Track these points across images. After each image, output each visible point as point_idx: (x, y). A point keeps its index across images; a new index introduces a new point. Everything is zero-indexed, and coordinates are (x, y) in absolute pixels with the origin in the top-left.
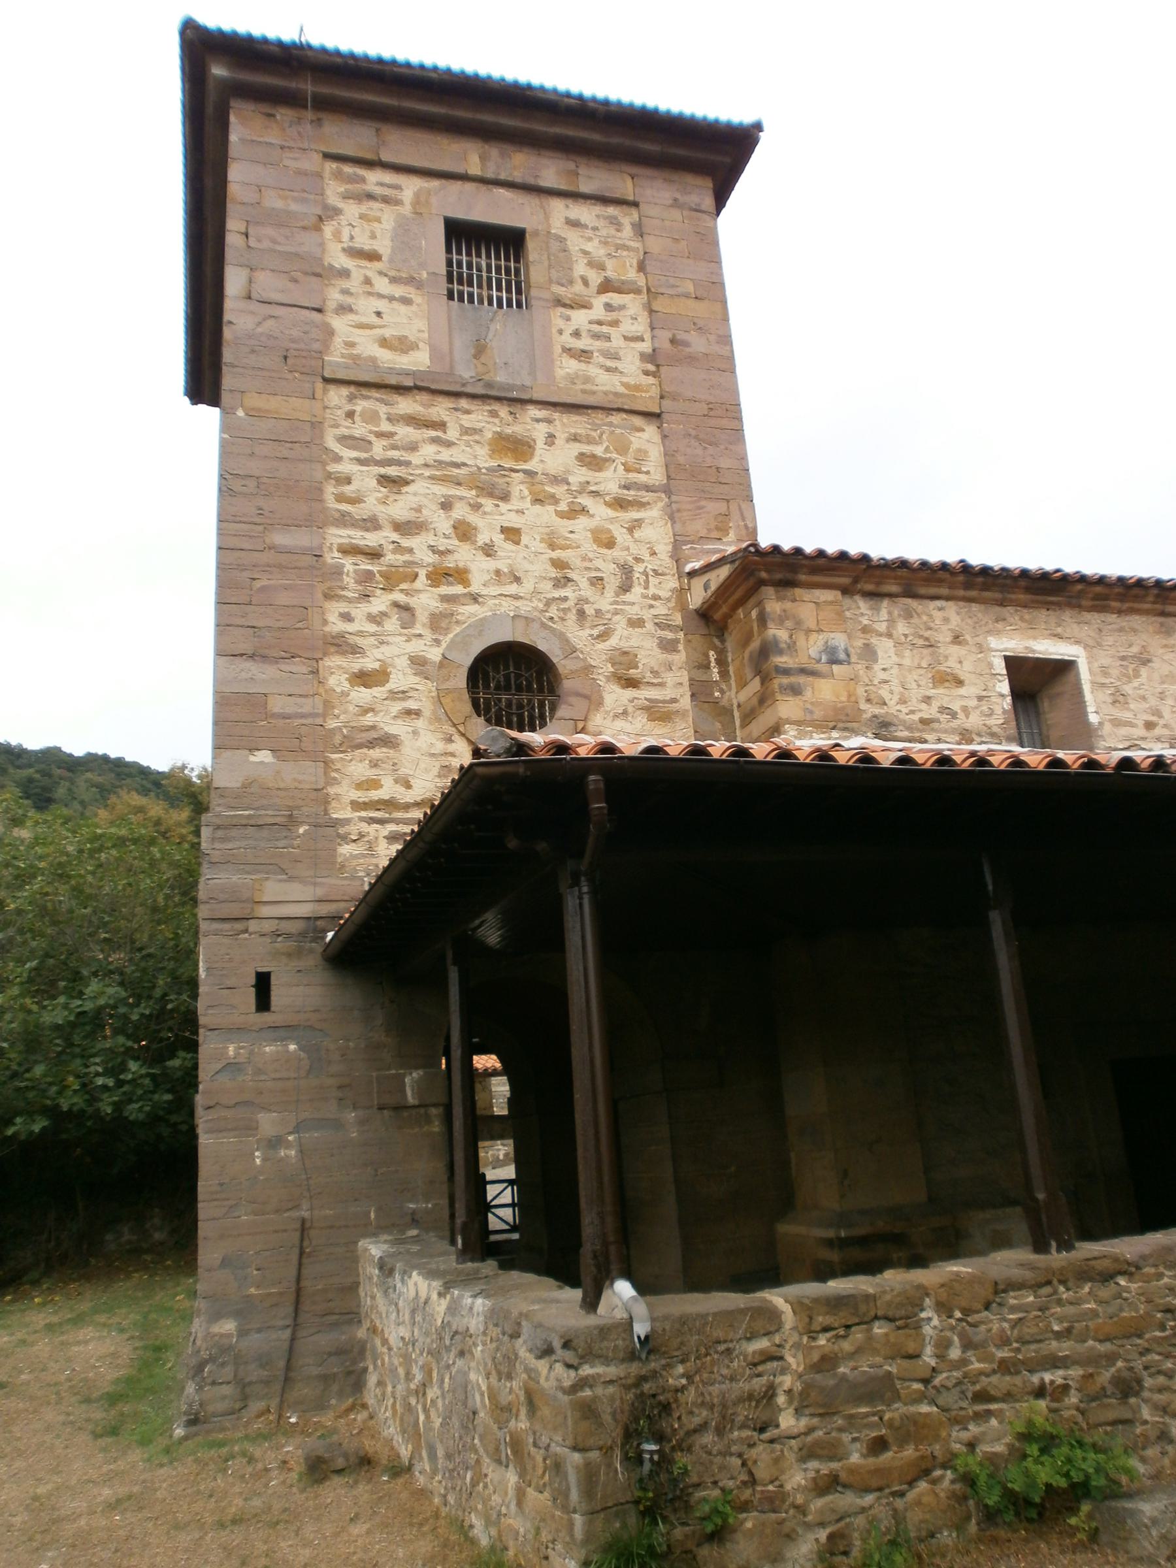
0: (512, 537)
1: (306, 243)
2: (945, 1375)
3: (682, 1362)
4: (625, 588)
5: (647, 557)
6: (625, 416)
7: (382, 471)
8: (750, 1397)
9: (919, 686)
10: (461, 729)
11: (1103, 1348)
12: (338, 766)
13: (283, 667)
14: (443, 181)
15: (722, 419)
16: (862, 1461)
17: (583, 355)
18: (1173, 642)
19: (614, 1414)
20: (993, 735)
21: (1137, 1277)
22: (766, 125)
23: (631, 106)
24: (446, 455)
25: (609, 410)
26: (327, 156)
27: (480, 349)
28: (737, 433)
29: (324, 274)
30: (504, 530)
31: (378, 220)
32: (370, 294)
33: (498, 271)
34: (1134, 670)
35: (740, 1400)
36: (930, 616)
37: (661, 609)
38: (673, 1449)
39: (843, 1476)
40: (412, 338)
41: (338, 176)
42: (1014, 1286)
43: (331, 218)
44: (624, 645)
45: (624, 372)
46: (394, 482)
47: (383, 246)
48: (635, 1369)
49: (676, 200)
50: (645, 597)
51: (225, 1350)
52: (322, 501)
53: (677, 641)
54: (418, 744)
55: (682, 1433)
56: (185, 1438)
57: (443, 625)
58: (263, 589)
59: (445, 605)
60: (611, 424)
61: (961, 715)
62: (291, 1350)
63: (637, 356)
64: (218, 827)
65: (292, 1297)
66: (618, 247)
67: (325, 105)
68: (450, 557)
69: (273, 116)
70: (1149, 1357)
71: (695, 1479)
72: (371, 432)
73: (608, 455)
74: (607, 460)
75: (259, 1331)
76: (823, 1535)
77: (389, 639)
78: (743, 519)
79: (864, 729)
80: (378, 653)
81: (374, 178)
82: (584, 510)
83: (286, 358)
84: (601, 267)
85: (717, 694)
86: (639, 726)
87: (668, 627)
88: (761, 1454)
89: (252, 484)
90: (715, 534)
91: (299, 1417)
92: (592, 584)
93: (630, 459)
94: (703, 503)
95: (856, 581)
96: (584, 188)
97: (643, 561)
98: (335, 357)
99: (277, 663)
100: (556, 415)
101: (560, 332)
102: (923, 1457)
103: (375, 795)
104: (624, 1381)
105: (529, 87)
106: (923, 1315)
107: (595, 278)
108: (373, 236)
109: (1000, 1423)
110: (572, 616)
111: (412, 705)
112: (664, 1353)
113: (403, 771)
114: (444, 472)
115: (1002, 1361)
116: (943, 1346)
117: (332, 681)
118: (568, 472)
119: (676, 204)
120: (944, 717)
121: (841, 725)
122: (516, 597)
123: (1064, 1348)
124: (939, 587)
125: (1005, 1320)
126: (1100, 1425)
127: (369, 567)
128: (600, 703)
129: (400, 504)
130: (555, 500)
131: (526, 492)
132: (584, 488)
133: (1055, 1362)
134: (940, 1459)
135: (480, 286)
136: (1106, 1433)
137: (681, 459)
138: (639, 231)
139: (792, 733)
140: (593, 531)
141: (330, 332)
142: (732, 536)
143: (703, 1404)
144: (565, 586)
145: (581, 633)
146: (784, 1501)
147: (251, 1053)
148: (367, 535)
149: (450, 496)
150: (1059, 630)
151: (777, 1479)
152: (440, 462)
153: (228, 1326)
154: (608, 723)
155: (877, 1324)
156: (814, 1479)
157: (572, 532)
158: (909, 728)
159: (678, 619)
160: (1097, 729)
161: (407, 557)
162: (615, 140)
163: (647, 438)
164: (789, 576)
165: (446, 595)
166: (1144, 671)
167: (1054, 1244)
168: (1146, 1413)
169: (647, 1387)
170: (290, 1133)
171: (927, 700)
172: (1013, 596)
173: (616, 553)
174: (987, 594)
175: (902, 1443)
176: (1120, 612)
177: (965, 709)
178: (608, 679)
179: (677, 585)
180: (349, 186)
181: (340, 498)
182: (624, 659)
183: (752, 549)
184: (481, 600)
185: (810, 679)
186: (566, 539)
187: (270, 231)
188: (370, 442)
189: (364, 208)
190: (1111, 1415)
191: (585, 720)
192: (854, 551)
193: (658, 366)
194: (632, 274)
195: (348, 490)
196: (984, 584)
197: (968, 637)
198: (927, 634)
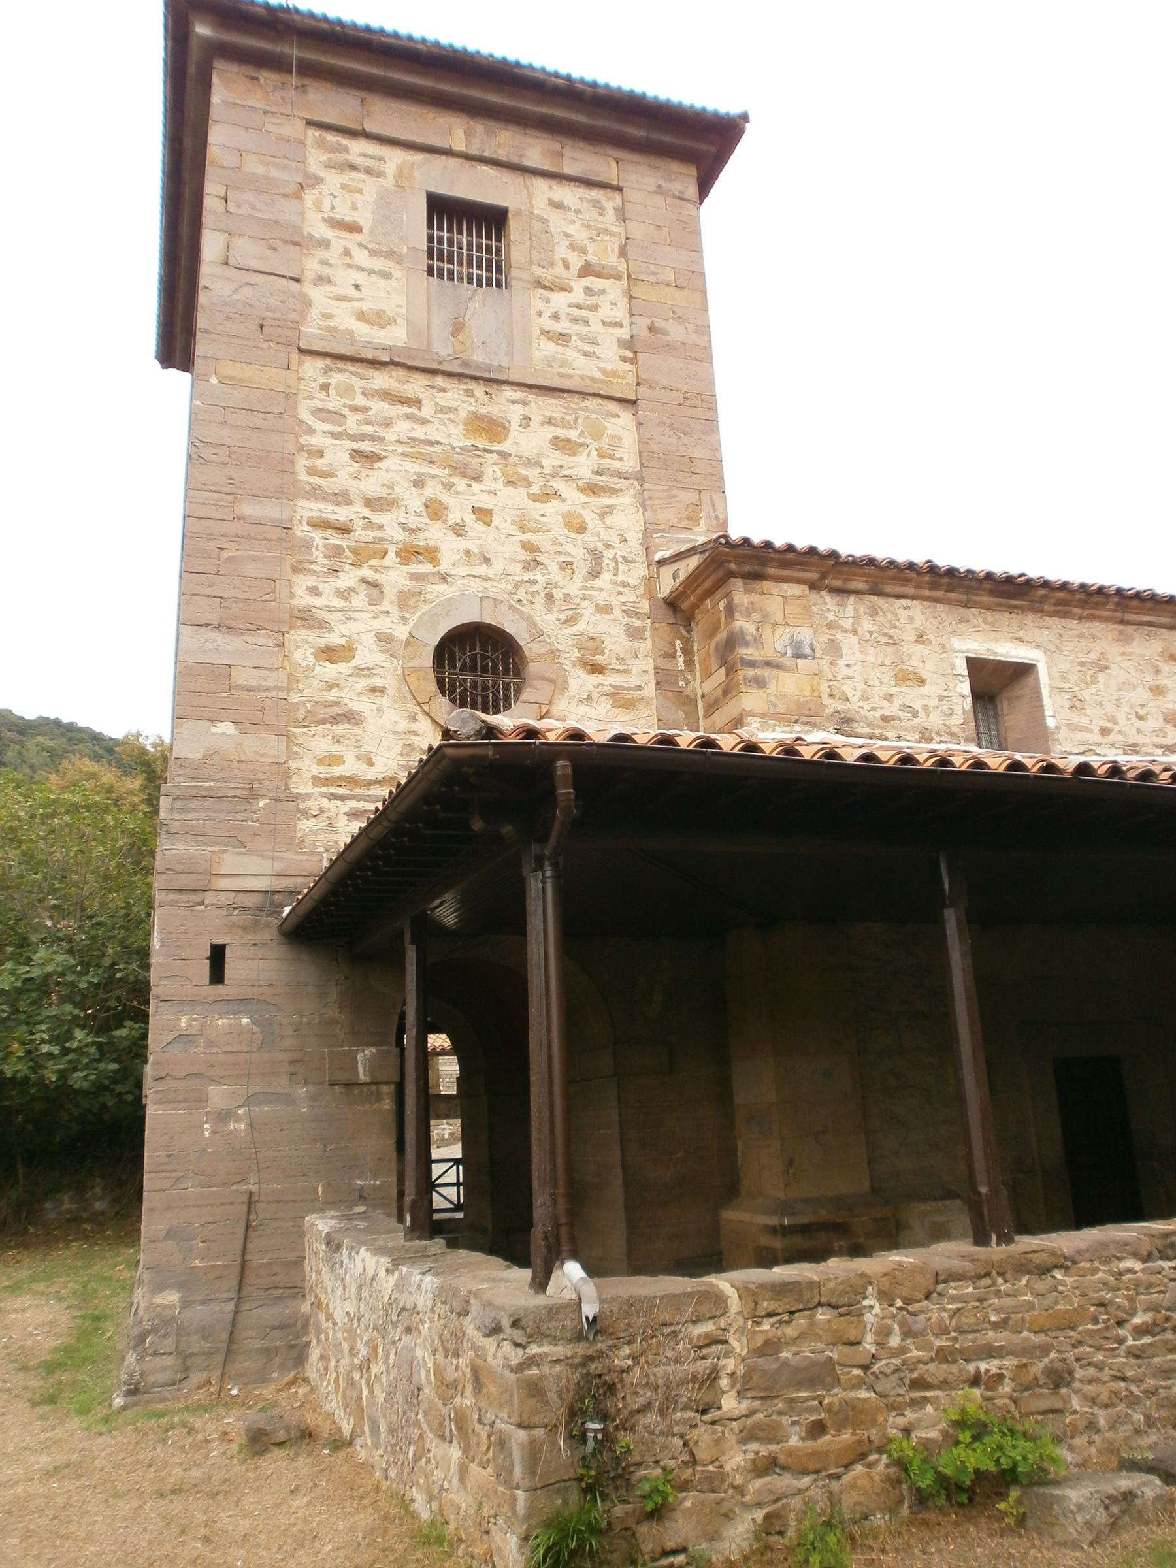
1: (287, 210)
2: (884, 1362)
3: (629, 1343)
4: (594, 574)
5: (617, 544)
8: (694, 1379)
9: (882, 683)
10: (426, 708)
13: (249, 639)
14: (428, 155)
15: (698, 408)
16: (800, 1444)
17: (562, 338)
19: (559, 1393)
20: (952, 734)
21: (1072, 1271)
24: (420, 432)
25: (584, 395)
26: (310, 123)
27: (458, 328)
28: (712, 424)
29: (300, 242)
30: (475, 510)
31: (360, 192)
36: (896, 615)
37: (629, 596)
39: (782, 1458)
40: (389, 313)
41: (321, 144)
43: (313, 186)
45: (602, 359)
46: (367, 457)
47: (364, 218)
48: (581, 1349)
49: (659, 186)
50: (614, 583)
51: (168, 1321)
53: (644, 629)
56: (125, 1408)
57: (411, 603)
59: (414, 583)
60: (586, 409)
64: (177, 798)
65: (237, 1271)
66: (600, 232)
67: (310, 71)
68: (420, 535)
69: (257, 79)
70: (1081, 1349)
71: (637, 1459)
73: (582, 440)
74: (581, 445)
75: (203, 1303)
76: (760, 1515)
78: (715, 511)
79: (826, 724)
80: (344, 629)
81: (357, 149)
82: (556, 494)
83: (261, 326)
85: (681, 683)
87: (636, 614)
88: (702, 1436)
89: (223, 453)
90: (685, 524)
91: (240, 1390)
92: (562, 569)
93: (604, 444)
94: (675, 492)
95: (824, 576)
96: (569, 170)
98: (312, 331)
100: (532, 398)
101: (539, 314)
102: (860, 1442)
103: (337, 771)
105: (518, 65)
106: (865, 1303)
107: (576, 262)
108: (354, 208)
109: (936, 1409)
110: (540, 600)
111: (377, 682)
112: (611, 1334)
113: (366, 748)
114: (418, 450)
115: (940, 1350)
116: (883, 1333)
117: (297, 655)
118: (541, 455)
119: (659, 190)
121: (803, 719)
122: (486, 579)
123: (1000, 1338)
125: (944, 1310)
126: (1032, 1414)
127: (339, 542)
128: (565, 688)
129: (372, 480)
131: (499, 474)
133: (991, 1352)
137: (655, 447)
138: (622, 215)
139: (755, 725)
141: (308, 303)
142: (703, 526)
145: (548, 617)
147: (203, 1025)
149: (423, 474)
150: (1021, 634)
152: (414, 439)
153: (172, 1297)
155: (820, 1310)
156: (754, 1461)
159: (645, 607)
160: (1053, 733)
161: (377, 534)
162: (602, 123)
163: (622, 424)
164: (757, 568)
166: (1101, 677)
167: (994, 1237)
168: (1076, 1403)
169: (592, 1367)
171: (889, 697)
173: (587, 538)
176: (1080, 618)
179: (646, 573)
180: (332, 156)
181: (312, 471)
184: (449, 579)
185: (775, 672)
187: (249, 197)
188: (344, 416)
191: (550, 704)
193: (635, 353)
195: (320, 463)
196: (949, 584)
197: (931, 637)
198: (892, 632)
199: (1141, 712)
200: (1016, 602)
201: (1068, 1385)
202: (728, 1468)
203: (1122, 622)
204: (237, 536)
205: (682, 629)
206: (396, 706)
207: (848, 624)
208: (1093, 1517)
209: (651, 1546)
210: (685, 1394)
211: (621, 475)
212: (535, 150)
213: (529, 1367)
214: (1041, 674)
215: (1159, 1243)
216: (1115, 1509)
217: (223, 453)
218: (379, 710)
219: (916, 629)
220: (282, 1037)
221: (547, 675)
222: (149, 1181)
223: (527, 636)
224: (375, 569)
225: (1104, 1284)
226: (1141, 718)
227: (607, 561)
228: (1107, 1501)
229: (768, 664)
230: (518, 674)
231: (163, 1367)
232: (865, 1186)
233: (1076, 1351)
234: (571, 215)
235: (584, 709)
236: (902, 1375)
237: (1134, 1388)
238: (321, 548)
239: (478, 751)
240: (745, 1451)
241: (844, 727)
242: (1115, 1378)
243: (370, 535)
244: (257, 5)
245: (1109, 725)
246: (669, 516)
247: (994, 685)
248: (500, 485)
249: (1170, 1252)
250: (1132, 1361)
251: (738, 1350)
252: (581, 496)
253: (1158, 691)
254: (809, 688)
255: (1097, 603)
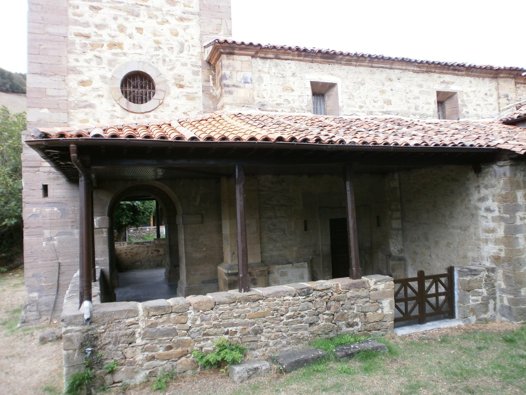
4: (181, 52)
8: (126, 335)
10: (118, 102)
11: (250, 321)
16: (163, 352)
19: (78, 340)
20: (302, 109)
35: (122, 336)
36: (285, 66)
37: (194, 59)
38: (98, 349)
39: (156, 356)
46: (95, 8)
48: (86, 327)
50: (188, 55)
51: (34, 302)
52: (67, 15)
53: (199, 71)
56: (20, 327)
57: (113, 64)
58: (44, 49)
59: (114, 57)
71: (105, 357)
75: (46, 296)
76: (148, 372)
85: (211, 91)
88: (129, 352)
92: (169, 50)
95: (257, 53)
110: (161, 61)
111: (100, 93)
120: (285, 103)
121: (246, 105)
122: (140, 54)
123: (238, 321)
125: (217, 313)
127: (86, 42)
128: (169, 94)
131: (146, 14)
133: (233, 325)
142: (222, 33)
147: (41, 211)
148: (85, 29)
150: (332, 72)
153: (35, 295)
159: (200, 63)
161: (100, 38)
164: (232, 51)
166: (362, 87)
167: (243, 290)
168: (263, 339)
169: (90, 332)
173: (179, 38)
174: (307, 59)
175: (177, 347)
176: (356, 66)
181: (75, 14)
183: (217, 41)
185: (237, 88)
191: (163, 99)
196: (305, 55)
197: (297, 74)
198: (282, 73)
199: (376, 100)
200: (330, 61)
203: (372, 67)
205: (212, 71)
210: (123, 339)
211: (192, 14)
213: (67, 333)
216: (251, 373)
218: (101, 103)
220: (68, 214)
224: (99, 52)
226: (375, 102)
229: (234, 86)
230: (154, 88)
231: (32, 315)
232: (260, 261)
237: (284, 334)
239: (39, 143)
241: (262, 108)
242: (277, 331)
245: (363, 105)
252: (177, 22)
253: (383, 92)
255: (362, 60)
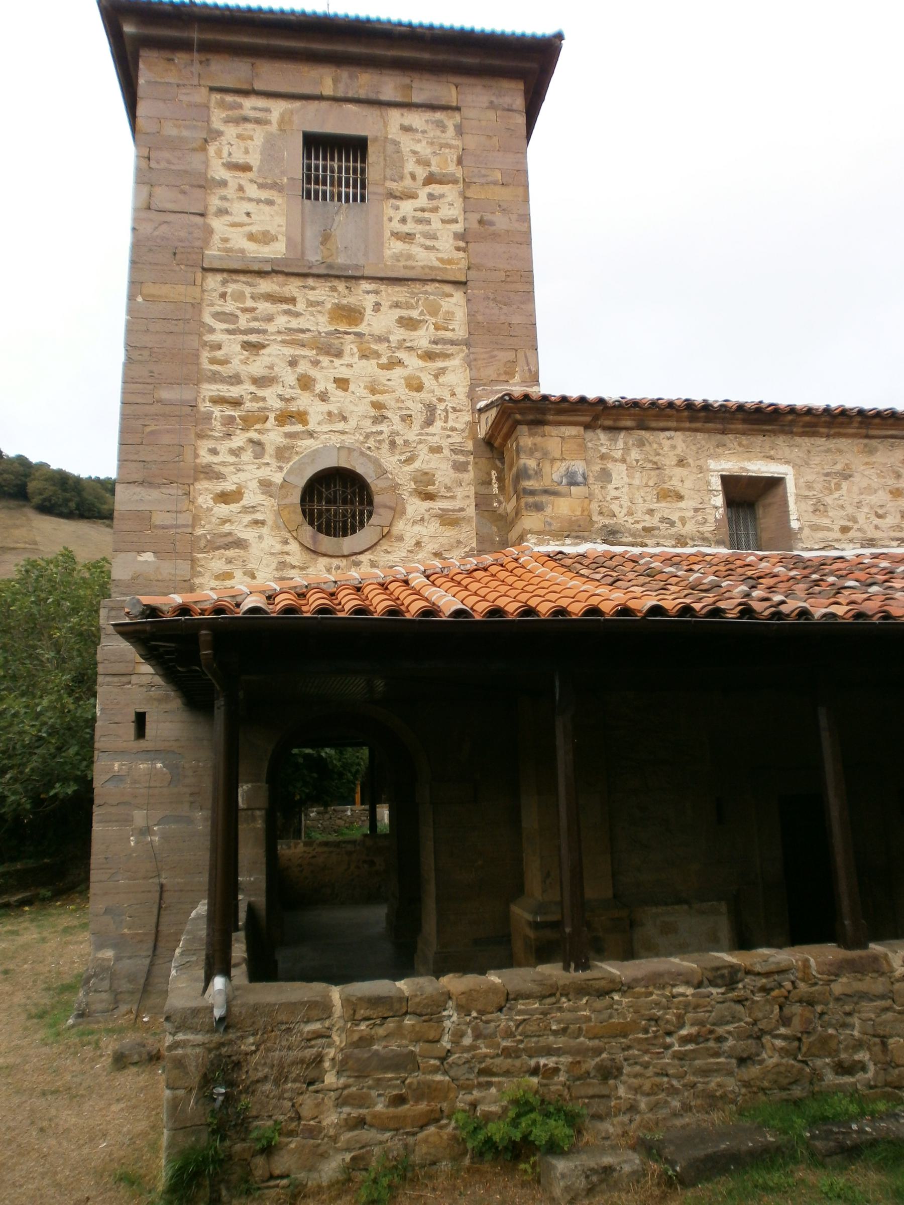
0: (341, 385)
1: (195, 161)
2: (457, 1055)
3: (253, 1035)
4: (429, 422)
5: (447, 397)
6: (437, 285)
7: (245, 338)
8: (302, 1061)
9: (645, 501)
12: (203, 563)
13: (164, 490)
14: (304, 102)
15: (518, 283)
16: (385, 1110)
17: (408, 237)
18: (874, 460)
19: (197, 1067)
20: (704, 539)
21: (627, 994)
22: (566, 36)
23: (452, 28)
24: (295, 323)
25: (424, 281)
26: (213, 89)
27: (326, 238)
28: (529, 295)
29: (205, 184)
30: (337, 381)
31: (251, 138)
32: (242, 198)
33: (347, 172)
34: (835, 484)
35: (293, 1063)
36: (660, 444)
37: (456, 438)
38: (241, 1092)
39: (368, 1119)
40: (273, 232)
41: (222, 105)
42: (519, 996)
43: (215, 139)
44: (425, 467)
45: (441, 249)
47: (254, 159)
48: (217, 1038)
49: (492, 102)
50: (444, 429)
52: (198, 364)
53: (468, 463)
54: (262, 545)
55: (248, 1082)
56: (73, 1026)
57: (286, 455)
58: (152, 433)
59: (288, 440)
60: (426, 292)
61: (678, 524)
62: (149, 972)
63: (452, 235)
64: (112, 609)
65: (153, 937)
66: (442, 146)
67: (209, 48)
68: (294, 403)
69: (173, 60)
70: (631, 1052)
71: (254, 1113)
72: (238, 308)
73: (422, 318)
74: (421, 321)
75: (130, 958)
76: (348, 1157)
77: (245, 467)
78: (528, 365)
79: (594, 536)
80: (235, 478)
81: (249, 104)
82: (400, 362)
83: (175, 254)
84: (427, 164)
85: (495, 504)
86: (433, 529)
87: (462, 452)
88: (307, 1103)
89: (146, 353)
90: (503, 378)
91: (150, 1018)
92: (403, 420)
93: (440, 320)
94: (495, 353)
95: (596, 418)
96: (416, 99)
97: (445, 401)
98: (213, 251)
99: (159, 488)
100: (383, 287)
101: (390, 219)
102: (432, 1111)
104: (207, 1046)
105: (368, 21)
106: (445, 1013)
107: (421, 173)
108: (247, 152)
109: (498, 1091)
110: (386, 446)
111: (259, 516)
112: (240, 1028)
113: (250, 566)
114: (293, 337)
115: (505, 1049)
116: (458, 1035)
117: (200, 500)
118: (389, 332)
119: (492, 106)
121: (574, 534)
122: (343, 433)
123: (559, 1042)
124: (668, 421)
125: (511, 1019)
126: (582, 1097)
127: (232, 413)
128: (403, 512)
129: (258, 363)
130: (378, 355)
131: (355, 350)
132: (401, 345)
133: (549, 1051)
134: (446, 1113)
135: (332, 185)
136: (584, 1104)
137: (480, 318)
138: (460, 131)
139: (533, 541)
140: (406, 379)
141: (210, 231)
142: (517, 378)
143: (265, 1064)
144: (382, 422)
145: (391, 459)
146: (320, 1132)
147: (130, 769)
148: (232, 388)
149: (297, 356)
150: (772, 452)
151: (317, 1117)
152: (290, 329)
153: (109, 954)
154: (408, 528)
155: (408, 1017)
156: (346, 1120)
157: (389, 380)
158: (633, 535)
159: (470, 446)
160: (796, 534)
161: (261, 404)
162: (441, 57)
163: (455, 303)
164: (539, 417)
165: (289, 433)
166: (845, 485)
167: (573, 965)
168: (622, 1091)
169: (224, 1050)
170: (155, 825)
171: (651, 512)
172: (732, 426)
173: (423, 395)
175: (417, 1100)
176: (828, 436)
177: (683, 520)
178: (411, 494)
179: (470, 419)
180: (230, 113)
181: (213, 361)
182: (425, 478)
183: (507, 398)
184: (315, 435)
185: (552, 498)
186: (384, 385)
187: (166, 155)
188: (237, 316)
189: (240, 129)
190: (591, 1092)
191: (390, 525)
192: (591, 395)
193: (467, 243)
194: (452, 168)
195: (219, 354)
197: (690, 461)
198: (655, 459)
199: (880, 512)
200: (769, 427)
201: (616, 1078)
202: (325, 1123)
204: (156, 415)
206: (273, 533)
207: (618, 454)
208: (573, 1184)
209: (261, 1172)
210: (295, 1071)
211: (453, 343)
212: (389, 86)
214: (788, 485)
215: (709, 974)
216: (595, 1179)
217: (146, 353)
219: (678, 455)
221: (388, 504)
222: (94, 876)
223: (373, 475)
224: (259, 431)
225: (656, 1004)
227: (439, 412)
228: (588, 1173)
230: (370, 503)
233: (626, 1053)
234: (419, 136)
235: (418, 528)
236: (472, 1065)
237: (675, 1082)
238: (219, 419)
239: (138, 627)
240: (340, 1113)
242: (657, 1074)
243: (256, 405)
244: (165, 4)
245: (850, 524)
246: (490, 372)
247: (748, 499)
248: (356, 359)
249: (719, 981)
250: (676, 1062)
251: (338, 1043)
254: (580, 509)
